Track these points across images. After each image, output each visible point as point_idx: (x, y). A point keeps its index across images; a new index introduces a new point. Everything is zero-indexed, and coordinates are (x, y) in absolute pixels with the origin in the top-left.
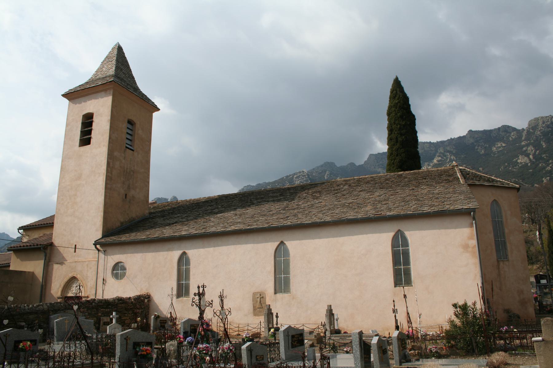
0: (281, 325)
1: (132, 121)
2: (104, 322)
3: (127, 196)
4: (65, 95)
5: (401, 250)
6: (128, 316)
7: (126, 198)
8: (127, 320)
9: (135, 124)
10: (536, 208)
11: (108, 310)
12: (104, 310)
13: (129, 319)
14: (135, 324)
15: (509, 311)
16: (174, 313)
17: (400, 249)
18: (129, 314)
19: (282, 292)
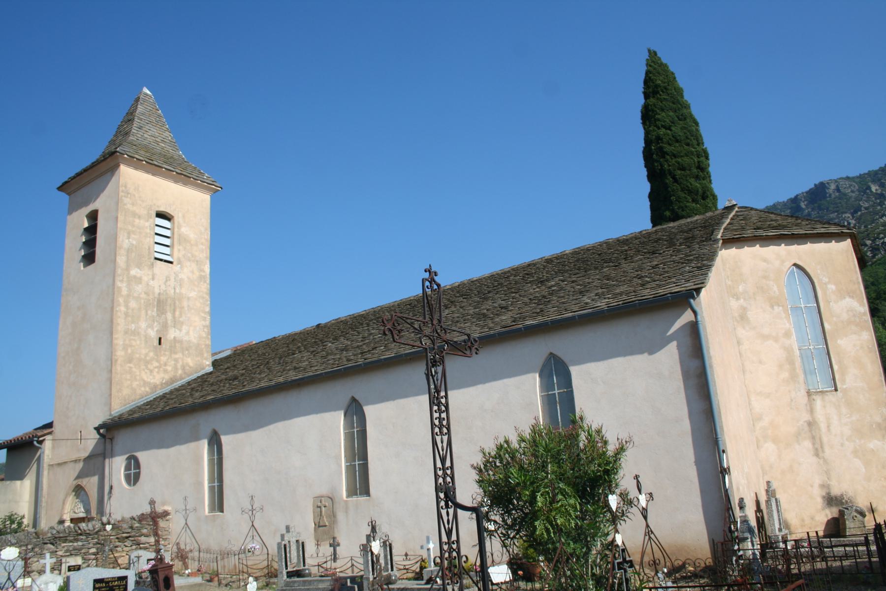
0: (352, 559)
1: (167, 213)
2: (69, 567)
3: (162, 340)
4: (60, 188)
5: (557, 394)
6: (123, 551)
7: (160, 343)
8: (122, 558)
9: (173, 217)
10: (542, 273)
11: (80, 543)
12: (71, 544)
13: (127, 554)
14: (26, 579)
15: (844, 501)
16: (194, 540)
17: (558, 393)
18: (126, 546)
19: (357, 495)
